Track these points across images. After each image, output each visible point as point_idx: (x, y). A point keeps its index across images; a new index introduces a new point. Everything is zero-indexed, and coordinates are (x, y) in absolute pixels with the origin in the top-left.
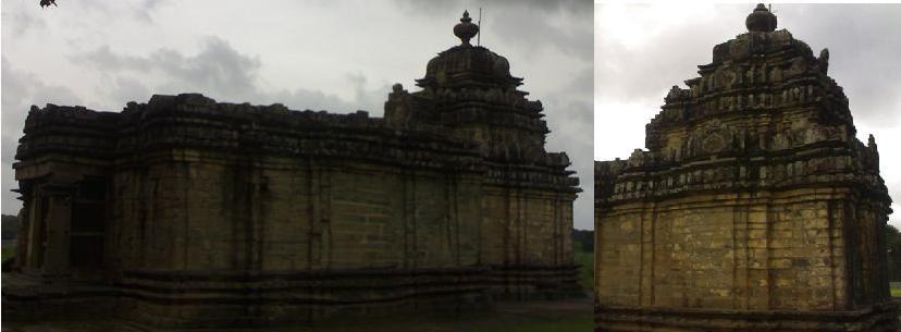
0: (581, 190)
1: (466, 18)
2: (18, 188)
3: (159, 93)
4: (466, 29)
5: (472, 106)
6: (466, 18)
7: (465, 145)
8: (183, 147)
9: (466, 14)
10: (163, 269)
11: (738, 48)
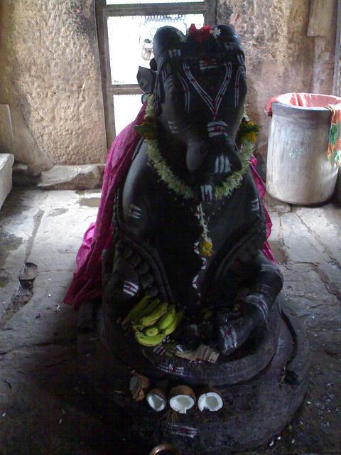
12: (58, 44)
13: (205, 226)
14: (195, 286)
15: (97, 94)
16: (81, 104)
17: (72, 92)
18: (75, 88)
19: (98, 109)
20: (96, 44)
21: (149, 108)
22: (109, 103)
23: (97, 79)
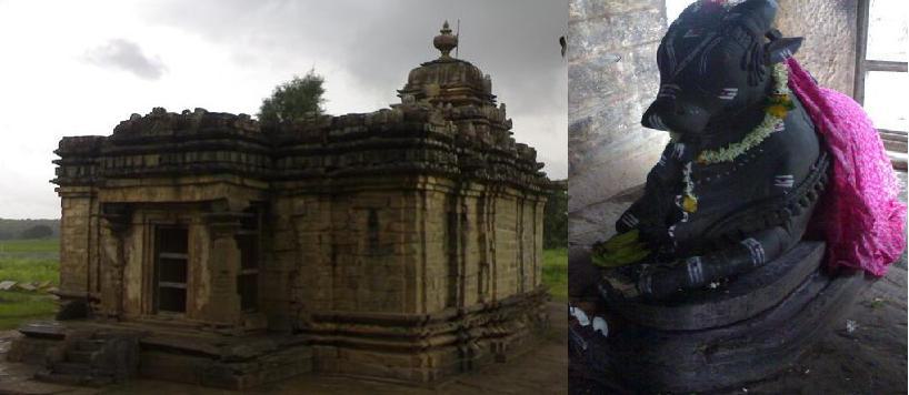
0: (54, 181)
1: (446, 30)
2: (826, 282)
3: (71, 134)
4: (445, 43)
5: (483, 124)
6: (446, 30)
7: (814, 167)
8: (426, 173)
9: (446, 26)
10: (396, 314)
11: (279, 102)
12: (816, 19)
13: (687, 179)
14: (671, 235)
15: (848, 68)
16: (830, 76)
17: (823, 64)
18: (827, 60)
19: (847, 81)
20: (854, 21)
21: (163, 182)
22: (860, 78)
23: (850, 54)
